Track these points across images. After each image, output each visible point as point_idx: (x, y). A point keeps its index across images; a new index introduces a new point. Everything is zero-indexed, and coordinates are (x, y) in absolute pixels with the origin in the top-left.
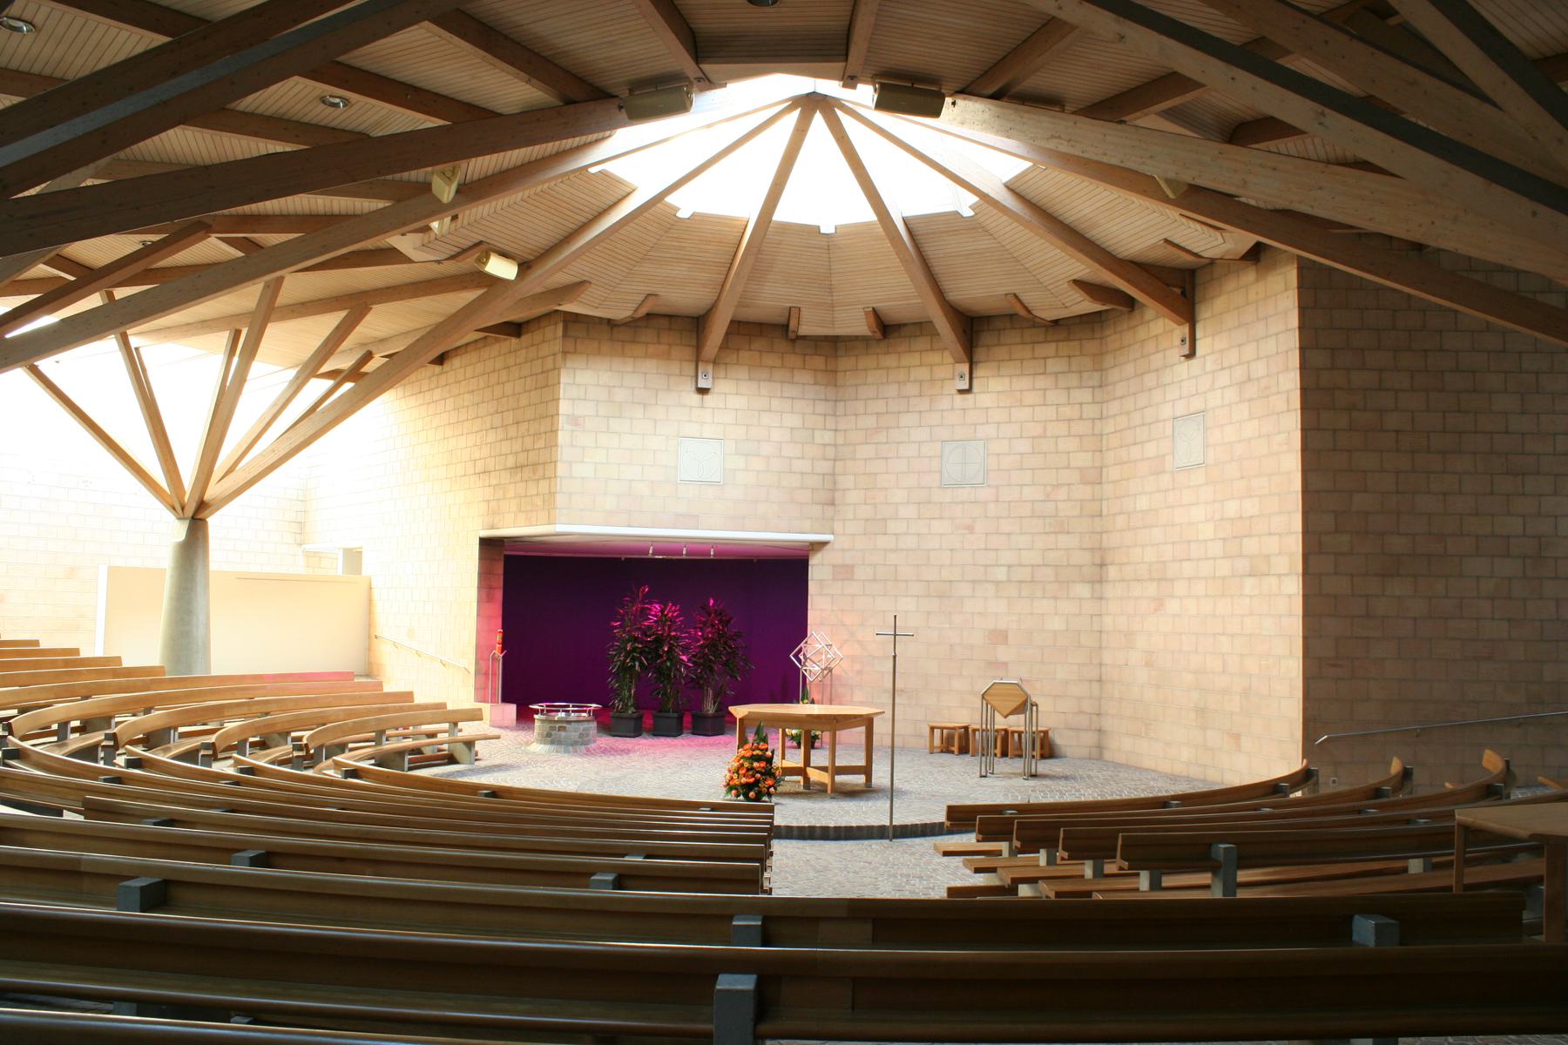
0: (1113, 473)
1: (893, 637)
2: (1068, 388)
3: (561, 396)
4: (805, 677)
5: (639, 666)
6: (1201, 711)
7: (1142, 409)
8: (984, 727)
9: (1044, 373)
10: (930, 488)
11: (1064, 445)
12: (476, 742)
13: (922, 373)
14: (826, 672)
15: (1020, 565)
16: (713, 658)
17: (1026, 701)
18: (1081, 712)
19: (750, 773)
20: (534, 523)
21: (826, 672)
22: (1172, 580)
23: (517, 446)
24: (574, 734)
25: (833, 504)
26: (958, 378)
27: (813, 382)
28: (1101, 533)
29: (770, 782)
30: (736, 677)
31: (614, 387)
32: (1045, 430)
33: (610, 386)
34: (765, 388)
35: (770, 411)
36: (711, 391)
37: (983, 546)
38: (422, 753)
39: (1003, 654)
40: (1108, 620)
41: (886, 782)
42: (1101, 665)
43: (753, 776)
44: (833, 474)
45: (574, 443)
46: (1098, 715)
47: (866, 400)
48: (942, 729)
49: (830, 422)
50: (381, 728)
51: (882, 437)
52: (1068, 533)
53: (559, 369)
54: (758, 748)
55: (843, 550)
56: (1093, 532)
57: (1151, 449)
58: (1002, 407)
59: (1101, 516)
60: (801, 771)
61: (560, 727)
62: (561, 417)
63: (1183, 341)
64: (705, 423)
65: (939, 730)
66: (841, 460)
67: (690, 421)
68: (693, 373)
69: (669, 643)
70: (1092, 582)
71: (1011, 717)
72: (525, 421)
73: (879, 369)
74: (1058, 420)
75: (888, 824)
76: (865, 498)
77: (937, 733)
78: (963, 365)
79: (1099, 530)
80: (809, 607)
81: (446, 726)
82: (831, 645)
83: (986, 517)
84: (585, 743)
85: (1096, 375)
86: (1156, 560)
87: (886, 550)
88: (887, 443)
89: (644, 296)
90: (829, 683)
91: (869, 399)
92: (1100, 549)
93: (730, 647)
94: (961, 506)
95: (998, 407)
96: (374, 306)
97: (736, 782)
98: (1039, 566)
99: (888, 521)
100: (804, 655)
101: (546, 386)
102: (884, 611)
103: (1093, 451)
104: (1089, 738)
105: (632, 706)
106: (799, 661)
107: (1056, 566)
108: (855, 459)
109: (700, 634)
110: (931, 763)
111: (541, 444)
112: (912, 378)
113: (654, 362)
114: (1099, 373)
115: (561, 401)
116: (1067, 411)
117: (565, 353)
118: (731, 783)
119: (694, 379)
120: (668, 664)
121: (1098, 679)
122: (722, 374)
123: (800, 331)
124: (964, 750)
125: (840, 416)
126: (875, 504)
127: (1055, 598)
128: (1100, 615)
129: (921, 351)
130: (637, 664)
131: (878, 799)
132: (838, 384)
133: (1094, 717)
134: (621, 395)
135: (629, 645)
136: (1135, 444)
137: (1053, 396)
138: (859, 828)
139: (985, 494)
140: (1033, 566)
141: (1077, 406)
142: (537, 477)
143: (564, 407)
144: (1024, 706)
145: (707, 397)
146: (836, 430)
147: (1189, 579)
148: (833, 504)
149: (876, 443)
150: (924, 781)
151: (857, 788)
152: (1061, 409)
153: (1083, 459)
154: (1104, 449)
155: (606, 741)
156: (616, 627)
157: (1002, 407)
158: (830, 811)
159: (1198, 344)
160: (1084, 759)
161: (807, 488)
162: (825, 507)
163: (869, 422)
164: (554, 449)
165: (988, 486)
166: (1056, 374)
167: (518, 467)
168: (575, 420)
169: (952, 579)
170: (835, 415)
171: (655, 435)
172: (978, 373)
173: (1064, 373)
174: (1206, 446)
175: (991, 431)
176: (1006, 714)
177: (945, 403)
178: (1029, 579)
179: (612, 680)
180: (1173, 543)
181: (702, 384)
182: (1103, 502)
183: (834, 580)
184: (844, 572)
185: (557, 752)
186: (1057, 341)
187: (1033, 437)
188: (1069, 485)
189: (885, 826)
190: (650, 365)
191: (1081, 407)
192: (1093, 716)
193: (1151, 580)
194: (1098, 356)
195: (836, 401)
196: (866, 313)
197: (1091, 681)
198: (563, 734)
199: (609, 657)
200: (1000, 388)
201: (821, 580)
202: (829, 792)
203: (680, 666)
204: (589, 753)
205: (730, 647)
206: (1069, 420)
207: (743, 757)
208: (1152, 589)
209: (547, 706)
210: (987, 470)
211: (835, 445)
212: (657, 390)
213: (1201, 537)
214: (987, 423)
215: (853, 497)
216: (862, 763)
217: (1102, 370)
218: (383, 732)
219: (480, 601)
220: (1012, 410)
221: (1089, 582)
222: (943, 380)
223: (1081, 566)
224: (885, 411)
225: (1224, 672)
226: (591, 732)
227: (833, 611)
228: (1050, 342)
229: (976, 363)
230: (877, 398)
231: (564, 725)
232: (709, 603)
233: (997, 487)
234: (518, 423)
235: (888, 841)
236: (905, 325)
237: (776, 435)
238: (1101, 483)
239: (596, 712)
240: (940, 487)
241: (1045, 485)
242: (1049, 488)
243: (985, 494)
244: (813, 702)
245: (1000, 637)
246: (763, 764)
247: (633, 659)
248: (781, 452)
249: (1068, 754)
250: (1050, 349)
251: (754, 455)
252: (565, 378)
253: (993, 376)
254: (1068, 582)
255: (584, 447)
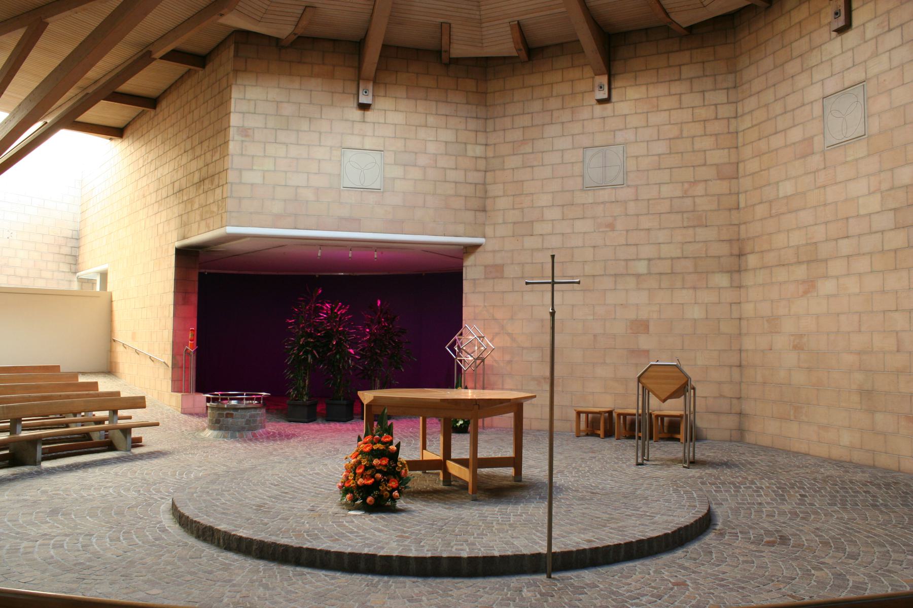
0: (752, 166)
1: (550, 285)
2: (703, 92)
3: (232, 109)
4: (460, 368)
5: (312, 358)
6: (867, 394)
7: (784, 97)
8: (640, 411)
9: (679, 79)
10: (573, 191)
11: (700, 144)
12: (132, 429)
13: (565, 88)
14: (478, 362)
15: (659, 258)
16: (379, 352)
17: (686, 384)
18: (722, 396)
19: (369, 472)
20: (211, 229)
21: (478, 362)
22: (826, 261)
23: (201, 163)
24: (240, 420)
25: (484, 210)
26: (597, 89)
27: (465, 102)
28: (739, 225)
29: (393, 484)
30: (400, 368)
31: (281, 102)
32: (681, 131)
33: (277, 102)
34: (421, 106)
35: (426, 126)
36: (372, 107)
37: (625, 243)
38: (91, 439)
39: (644, 342)
40: (748, 309)
41: (543, 475)
42: (740, 351)
43: (372, 476)
44: (484, 184)
45: (244, 153)
46: (739, 398)
47: (513, 116)
48: (587, 413)
49: (481, 138)
50: (16, 415)
51: (528, 149)
52: (706, 226)
53: (231, 86)
54: (379, 441)
55: (494, 251)
56: (731, 225)
57: (796, 135)
58: (640, 113)
59: (738, 208)
60: (440, 465)
61: (227, 414)
62: (231, 129)
63: (836, 14)
64: (366, 136)
65: (584, 415)
66: (491, 171)
67: (353, 134)
68: (354, 91)
69: (338, 337)
70: (730, 272)
71: (669, 401)
72: (206, 140)
73: (525, 88)
74: (693, 122)
75: (544, 550)
76: (513, 204)
77: (583, 416)
78: (601, 77)
79: (736, 222)
80: (464, 304)
81: (105, 414)
82: (483, 337)
83: (627, 215)
84: (251, 429)
85: (731, 77)
86: (804, 242)
87: (532, 250)
88: (533, 153)
89: (303, 8)
90: (482, 372)
91: (516, 115)
92: (738, 240)
93: (394, 342)
94: (602, 206)
95: (636, 113)
96: (49, 20)
97: (352, 483)
98: (678, 258)
99: (535, 223)
100: (459, 347)
101: (221, 105)
102: (532, 306)
103: (729, 148)
104: (729, 422)
105: (306, 394)
106: (454, 352)
107: (695, 258)
108: (504, 169)
109: (368, 330)
110: (581, 448)
111: (217, 156)
112: (554, 93)
113: (319, 80)
114: (733, 75)
115: (232, 114)
116: (703, 113)
117: (236, 71)
118: (347, 485)
119: (356, 96)
120: (338, 356)
121: (738, 364)
122: (382, 93)
123: (452, 51)
124: (609, 434)
125: (489, 132)
126: (522, 209)
127: (695, 288)
128: (739, 303)
129: (562, 69)
130: (310, 357)
131: (529, 500)
132: (488, 104)
133: (735, 401)
134: (288, 109)
135: (302, 340)
136: (776, 133)
137: (687, 99)
138: (504, 558)
139: (625, 193)
140: (672, 259)
141: (713, 107)
142: (213, 187)
143: (235, 120)
144: (683, 389)
145: (369, 114)
146: (486, 145)
147: (848, 257)
148: (484, 210)
149: (523, 154)
150: (579, 471)
151: (505, 483)
152: (697, 111)
153: (718, 156)
154: (740, 145)
155: (273, 426)
156: (291, 324)
157: (640, 113)
158: (467, 524)
159: (855, 15)
160: (725, 441)
161: (461, 196)
162: (478, 213)
163: (517, 135)
164: (226, 158)
165: (628, 186)
166: (691, 79)
167: (202, 181)
168: (245, 132)
169: (595, 274)
170: (486, 131)
171: (320, 146)
172: (615, 84)
173: (698, 77)
174: (867, 116)
175: (630, 135)
176: (663, 398)
177: (585, 113)
178: (670, 271)
179: (287, 372)
180: (826, 223)
181: (363, 100)
182: (740, 195)
183: (486, 278)
184: (495, 271)
185: (224, 437)
186: (691, 49)
187: (670, 139)
188: (706, 181)
189: (539, 554)
190: (314, 83)
191: (716, 108)
192: (732, 399)
193: (799, 263)
194: (733, 68)
195: (486, 119)
196: (512, 27)
197: (731, 366)
198: (230, 420)
199: (285, 350)
200: (637, 96)
201: (474, 280)
202: (470, 491)
203: (348, 359)
204: (255, 438)
205: (394, 342)
206: (705, 121)
207: (362, 453)
208: (801, 272)
209: (221, 395)
210: (627, 172)
211: (486, 158)
212: (321, 106)
213: (862, 212)
214: (626, 129)
215: (502, 203)
216: (510, 453)
217: (735, 72)
218: (19, 420)
219: (176, 304)
220: (649, 115)
221: (728, 272)
222: (583, 93)
223: (719, 257)
224: (531, 125)
225: (898, 351)
226: (258, 419)
227: (485, 306)
228: (684, 50)
229: (614, 75)
230: (523, 114)
231: (232, 412)
232: (377, 304)
233: (636, 187)
234: (202, 143)
235: (543, 577)
236: (547, 47)
237: (432, 148)
238: (737, 178)
239: (265, 398)
240: (582, 190)
241: (682, 183)
242: (686, 186)
243: (625, 193)
244: (466, 388)
245: (641, 326)
246: (385, 462)
247: (307, 352)
248: (436, 163)
249: (708, 437)
250: (685, 56)
251: (411, 166)
252: (235, 94)
253: (630, 86)
254: (707, 272)
255: (253, 156)
